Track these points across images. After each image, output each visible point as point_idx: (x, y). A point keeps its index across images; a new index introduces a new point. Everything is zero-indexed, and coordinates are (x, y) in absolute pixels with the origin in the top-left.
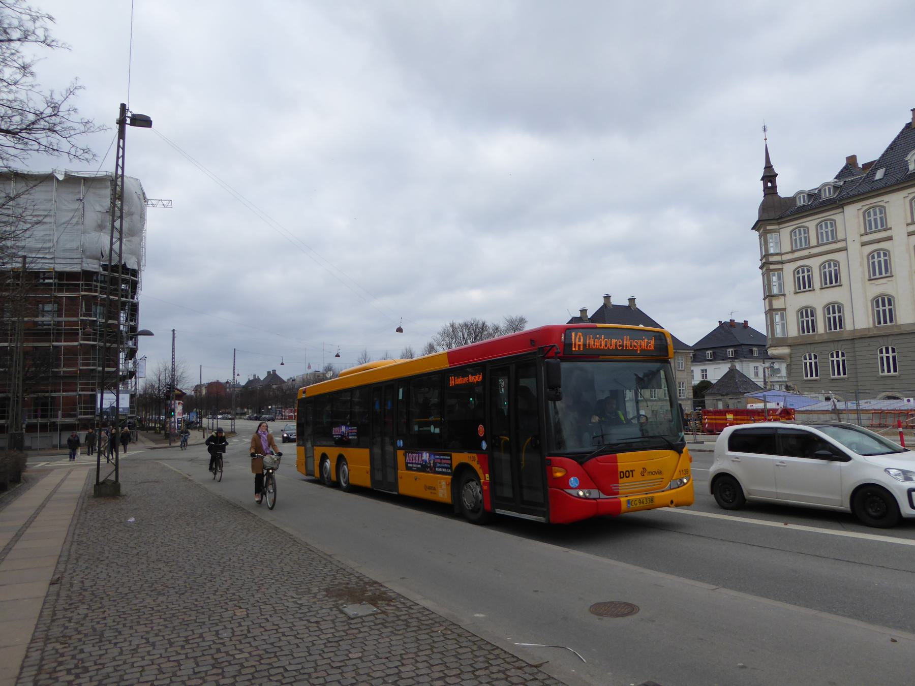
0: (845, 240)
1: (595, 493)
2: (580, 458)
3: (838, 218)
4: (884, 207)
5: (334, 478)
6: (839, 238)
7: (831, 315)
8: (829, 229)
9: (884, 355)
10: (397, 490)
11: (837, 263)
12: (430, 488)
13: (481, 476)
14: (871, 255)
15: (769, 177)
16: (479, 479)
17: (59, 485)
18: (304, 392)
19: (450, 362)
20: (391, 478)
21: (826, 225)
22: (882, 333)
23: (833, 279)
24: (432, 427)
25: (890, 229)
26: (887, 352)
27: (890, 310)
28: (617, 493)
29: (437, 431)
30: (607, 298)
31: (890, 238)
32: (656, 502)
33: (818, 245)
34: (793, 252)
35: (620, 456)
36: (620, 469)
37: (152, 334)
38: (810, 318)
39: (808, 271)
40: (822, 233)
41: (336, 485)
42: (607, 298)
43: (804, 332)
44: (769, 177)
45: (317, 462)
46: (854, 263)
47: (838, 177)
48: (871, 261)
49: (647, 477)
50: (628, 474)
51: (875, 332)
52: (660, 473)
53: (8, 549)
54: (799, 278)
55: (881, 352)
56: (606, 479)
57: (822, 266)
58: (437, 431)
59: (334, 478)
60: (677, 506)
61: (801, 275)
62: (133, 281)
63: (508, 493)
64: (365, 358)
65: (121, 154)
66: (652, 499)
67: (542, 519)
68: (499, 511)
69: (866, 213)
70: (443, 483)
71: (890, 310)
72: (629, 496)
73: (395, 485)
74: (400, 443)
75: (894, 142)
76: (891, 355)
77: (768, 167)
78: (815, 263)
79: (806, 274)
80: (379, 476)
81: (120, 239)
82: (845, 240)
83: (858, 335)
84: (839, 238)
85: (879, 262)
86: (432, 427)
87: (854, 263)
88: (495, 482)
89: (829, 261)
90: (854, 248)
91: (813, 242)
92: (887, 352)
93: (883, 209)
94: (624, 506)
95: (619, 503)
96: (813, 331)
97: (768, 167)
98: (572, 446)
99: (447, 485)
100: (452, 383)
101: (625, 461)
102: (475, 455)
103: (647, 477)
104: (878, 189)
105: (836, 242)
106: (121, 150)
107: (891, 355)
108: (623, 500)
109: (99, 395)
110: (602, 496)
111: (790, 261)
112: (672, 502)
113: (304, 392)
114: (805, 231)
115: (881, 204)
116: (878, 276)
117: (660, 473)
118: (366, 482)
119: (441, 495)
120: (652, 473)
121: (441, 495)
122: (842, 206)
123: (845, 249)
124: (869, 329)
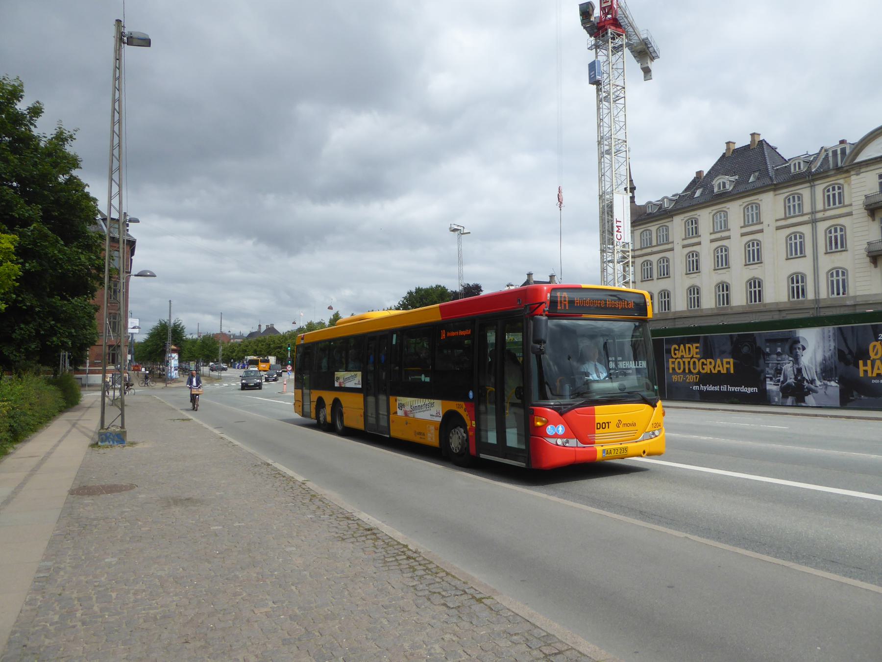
0: (851, 205)
1: (573, 442)
6: (846, 203)
7: (753, 290)
8: (797, 202)
10: (389, 434)
12: (420, 433)
13: (468, 422)
14: (747, 245)
17: (49, 454)
18: (303, 339)
19: (442, 315)
20: (383, 423)
21: (752, 207)
22: (692, 314)
23: (665, 273)
24: (423, 376)
27: (759, 291)
28: (594, 443)
29: (428, 379)
31: (728, 238)
32: (630, 452)
33: (657, 245)
34: (641, 249)
35: (598, 408)
36: (597, 421)
37: (155, 276)
38: (725, 292)
39: (801, 237)
40: (789, 207)
43: (793, 297)
46: (678, 260)
47: (686, 190)
48: (828, 235)
49: (622, 428)
50: (605, 425)
51: (688, 314)
52: (634, 425)
53: (7, 501)
54: (791, 244)
56: (584, 432)
57: (659, 261)
58: (428, 379)
60: (650, 455)
61: (793, 241)
65: (117, 104)
66: (626, 449)
67: (523, 465)
68: (482, 456)
69: (746, 208)
71: (759, 291)
72: (603, 447)
78: (654, 258)
79: (798, 240)
81: (120, 193)
82: (673, 242)
83: (677, 315)
85: (753, 250)
86: (423, 376)
87: (678, 260)
89: (721, 247)
90: (678, 248)
91: (654, 243)
93: (758, 207)
94: (599, 456)
95: (596, 451)
96: (760, 301)
99: (436, 429)
100: (443, 336)
101: (602, 413)
102: (462, 403)
103: (622, 428)
104: (693, 206)
105: (668, 244)
106: (117, 115)
108: (599, 449)
110: (580, 445)
111: (639, 256)
112: (644, 452)
113: (303, 339)
114: (799, 198)
117: (634, 425)
118: (359, 425)
119: (429, 439)
120: (626, 425)
121: (429, 439)
122: (672, 216)
123: (672, 250)
124: (742, 306)
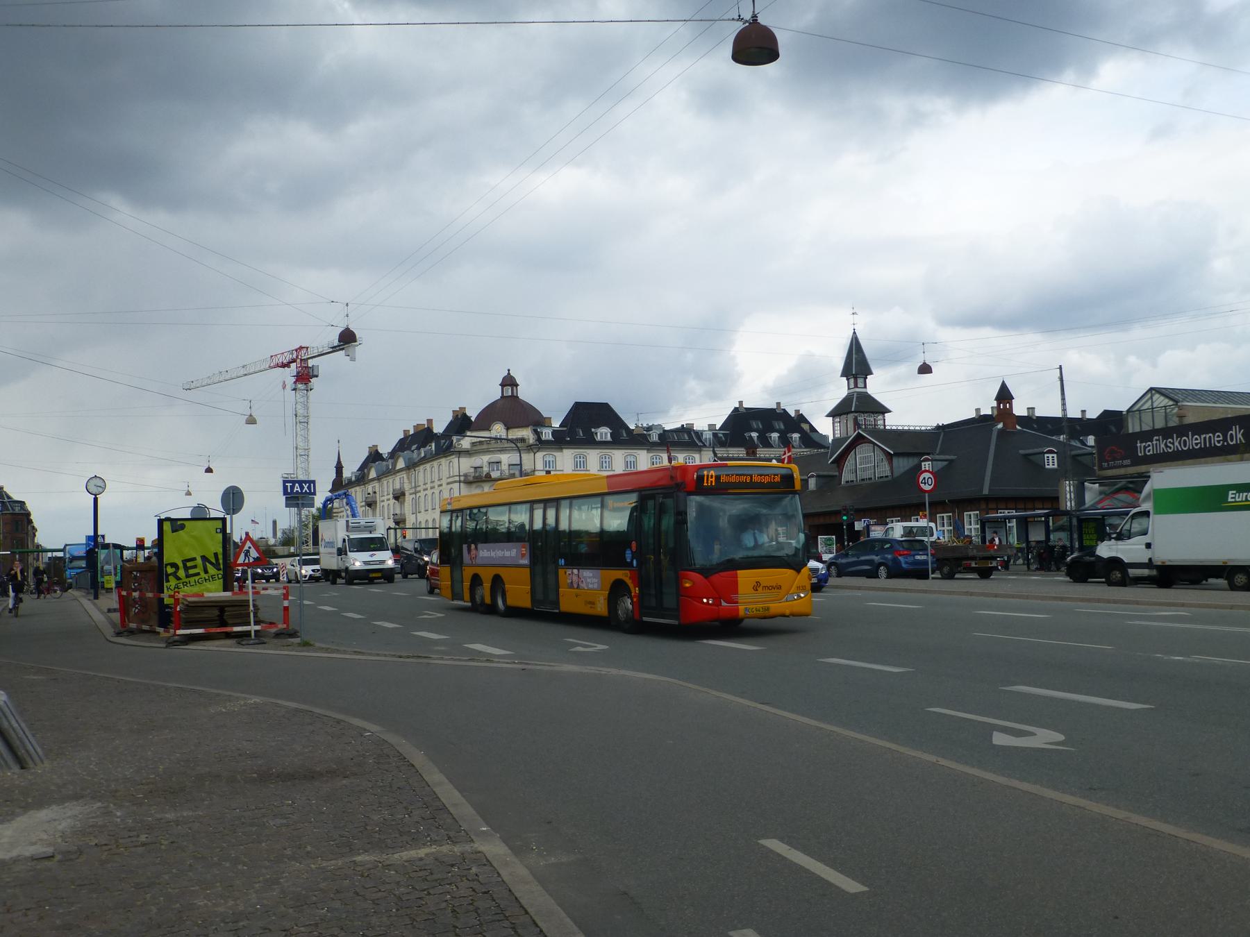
2: (706, 572)
3: (557, 454)
5: (488, 600)
15: (339, 468)
16: (630, 592)
30: (741, 403)
41: (491, 610)
42: (741, 403)
44: (339, 468)
45: (467, 584)
59: (488, 600)
63: (653, 602)
68: (645, 619)
70: (602, 598)
73: (556, 603)
74: (562, 562)
77: (339, 462)
80: (540, 596)
88: (641, 596)
97: (339, 462)
98: (699, 560)
109: (49, 554)
118: (526, 602)
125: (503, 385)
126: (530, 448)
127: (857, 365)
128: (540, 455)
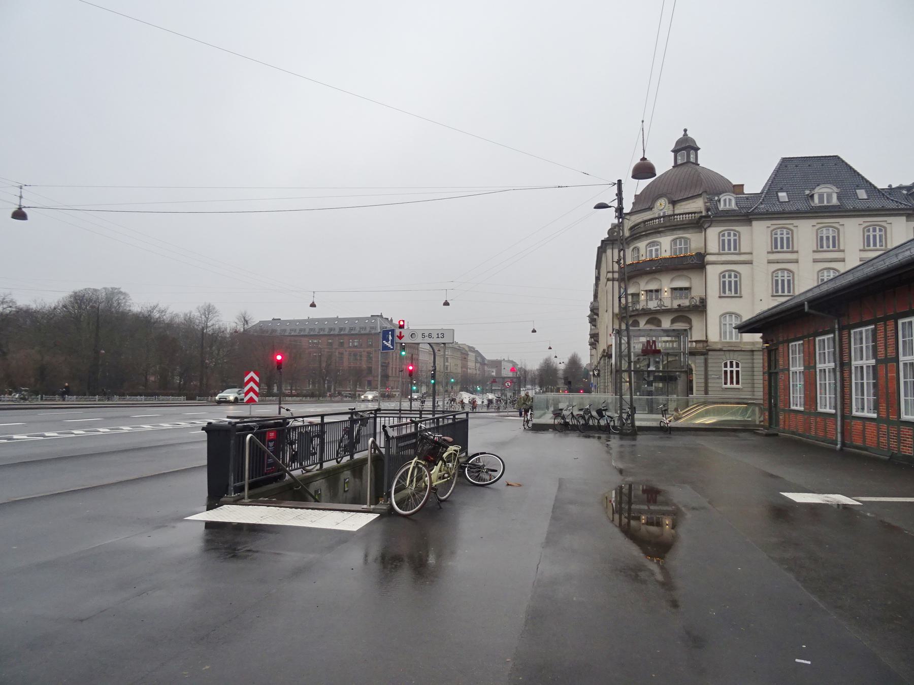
3: (743, 230)
4: (792, 231)
9: (729, 369)
11: (737, 274)
25: (797, 252)
26: (732, 366)
31: (797, 262)
34: (718, 254)
48: (722, 280)
55: (726, 366)
62: (372, 461)
64: (209, 311)
69: (866, 229)
75: (859, 174)
76: (735, 369)
84: (742, 251)
92: (732, 366)
107: (735, 369)
115: (884, 224)
116: (780, 293)
125: (676, 151)
126: (699, 223)
127: (685, 130)
128: (713, 233)
